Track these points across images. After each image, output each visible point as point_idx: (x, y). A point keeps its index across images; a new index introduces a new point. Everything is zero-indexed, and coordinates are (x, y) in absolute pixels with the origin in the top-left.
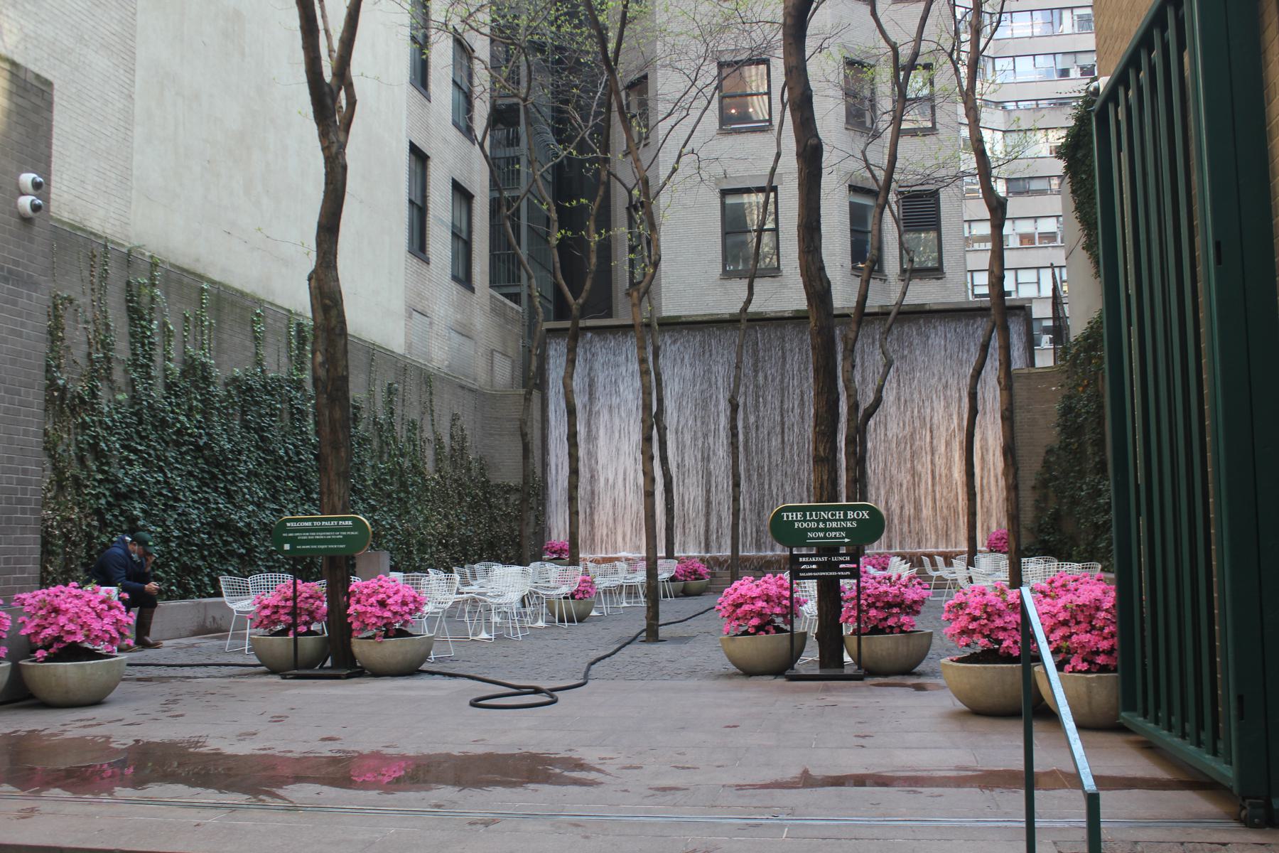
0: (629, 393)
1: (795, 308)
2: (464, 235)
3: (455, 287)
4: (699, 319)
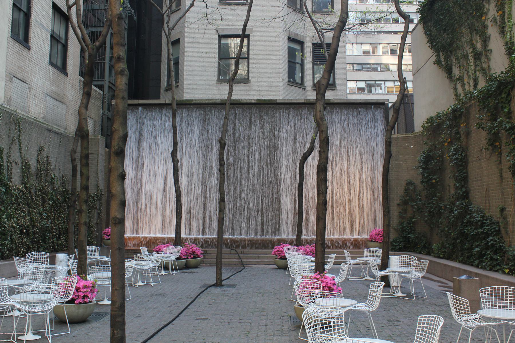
0: (165, 144)
1: (257, 98)
2: (24, 8)
3: (52, 70)
4: (204, 102)
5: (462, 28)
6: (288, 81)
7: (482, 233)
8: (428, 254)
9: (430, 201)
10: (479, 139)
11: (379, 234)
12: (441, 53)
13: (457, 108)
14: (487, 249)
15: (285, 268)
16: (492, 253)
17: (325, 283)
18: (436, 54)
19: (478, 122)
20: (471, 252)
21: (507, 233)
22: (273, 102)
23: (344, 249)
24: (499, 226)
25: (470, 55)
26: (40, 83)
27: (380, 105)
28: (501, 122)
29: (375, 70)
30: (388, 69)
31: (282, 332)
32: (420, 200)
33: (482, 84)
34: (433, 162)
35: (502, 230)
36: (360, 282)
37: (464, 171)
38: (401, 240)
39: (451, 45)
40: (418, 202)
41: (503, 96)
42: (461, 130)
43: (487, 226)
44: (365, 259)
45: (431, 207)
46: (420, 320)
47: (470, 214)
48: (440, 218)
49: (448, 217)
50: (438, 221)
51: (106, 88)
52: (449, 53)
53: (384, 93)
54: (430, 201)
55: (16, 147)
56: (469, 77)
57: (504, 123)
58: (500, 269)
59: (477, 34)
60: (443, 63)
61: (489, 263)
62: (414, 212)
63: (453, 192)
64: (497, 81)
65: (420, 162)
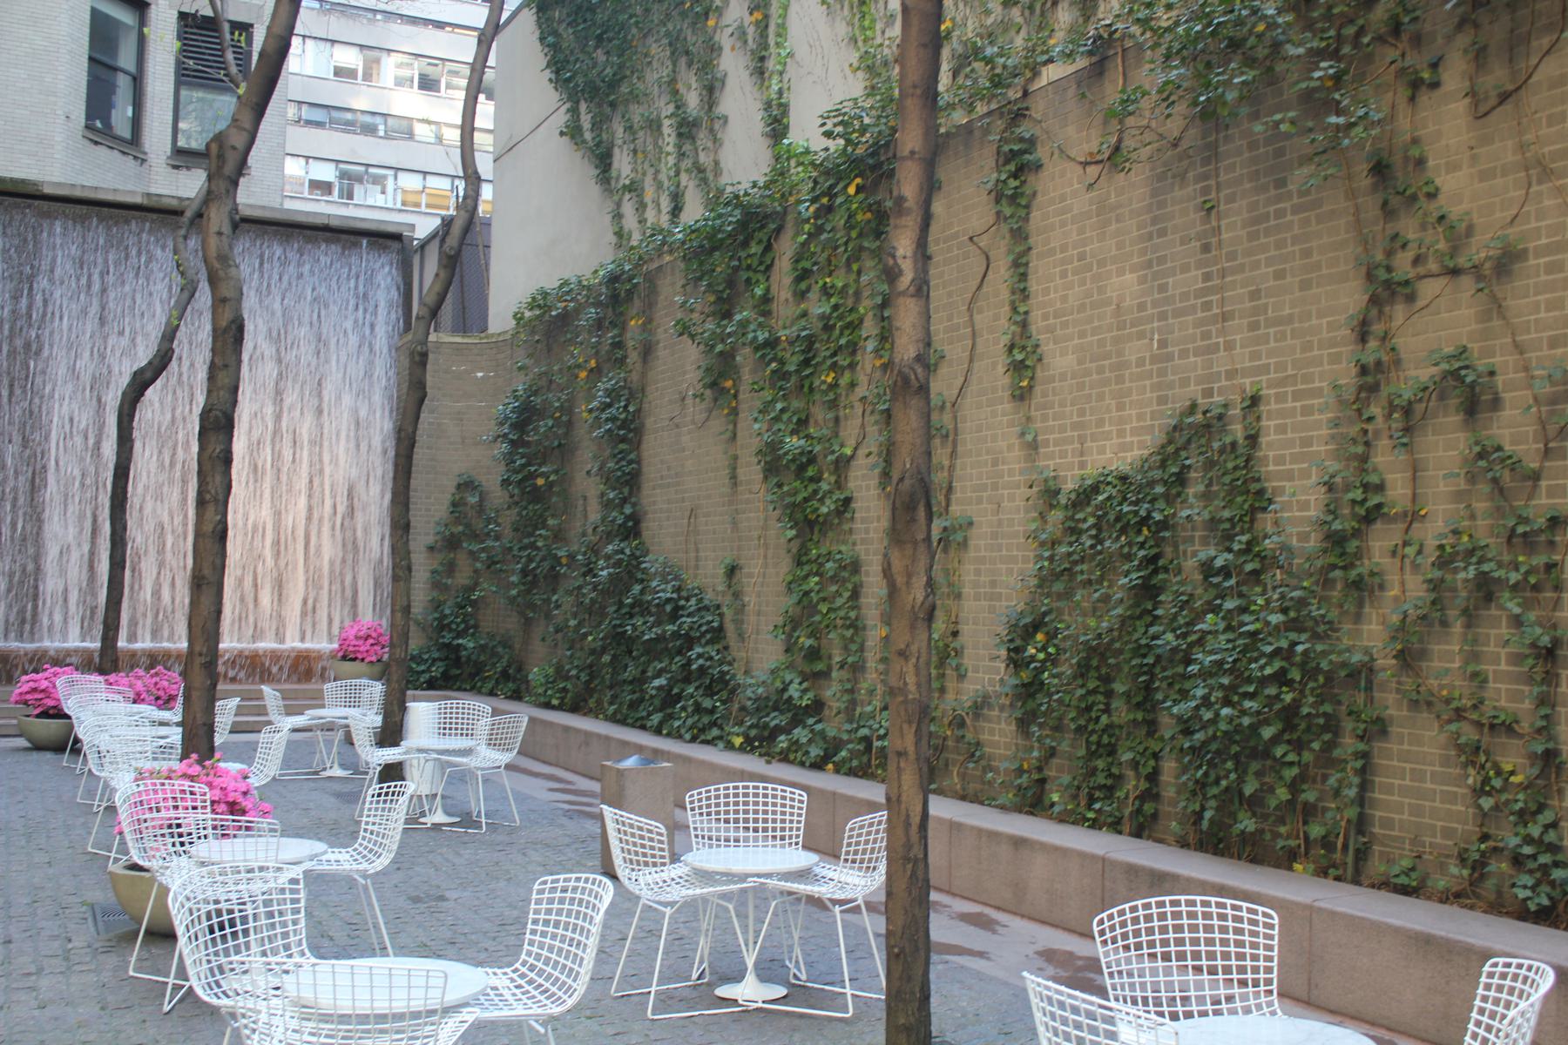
5: (650, 40)
6: (87, 127)
7: (676, 635)
8: (516, 696)
9: (526, 541)
10: (678, 367)
11: (368, 637)
12: (583, 106)
13: (624, 272)
14: (687, 680)
15: (67, 745)
16: (701, 692)
17: (217, 792)
18: (568, 105)
19: (679, 316)
20: (642, 691)
21: (741, 636)
22: (30, 190)
23: (262, 681)
24: (721, 615)
25: (666, 122)
27: (385, 239)
28: (744, 324)
29: (370, 130)
30: (410, 135)
31: (67, 959)
32: (497, 538)
33: (694, 211)
34: (544, 425)
35: (730, 627)
36: (312, 785)
37: (632, 456)
38: (436, 655)
39: (613, 84)
40: (490, 543)
41: (753, 251)
42: (629, 335)
43: (689, 615)
44: (330, 713)
45: (530, 559)
46: (541, 892)
47: (642, 581)
48: (554, 591)
49: (580, 588)
50: (548, 601)
52: (608, 110)
53: (390, 205)
54: (526, 541)
56: (659, 186)
57: (752, 327)
58: (720, 738)
59: (690, 64)
60: (588, 136)
61: (690, 722)
62: (476, 571)
63: (594, 516)
64: (739, 205)
65: (502, 424)
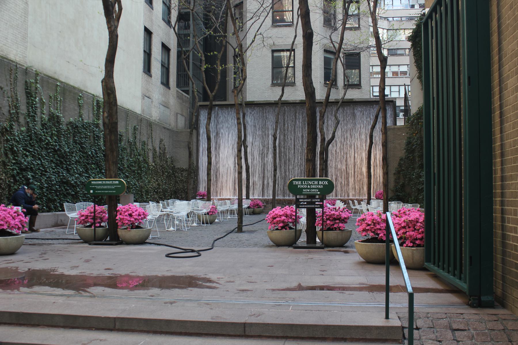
2: (166, 66)
3: (162, 87)
26: (157, 97)
51: (191, 92)
55: (150, 140)
